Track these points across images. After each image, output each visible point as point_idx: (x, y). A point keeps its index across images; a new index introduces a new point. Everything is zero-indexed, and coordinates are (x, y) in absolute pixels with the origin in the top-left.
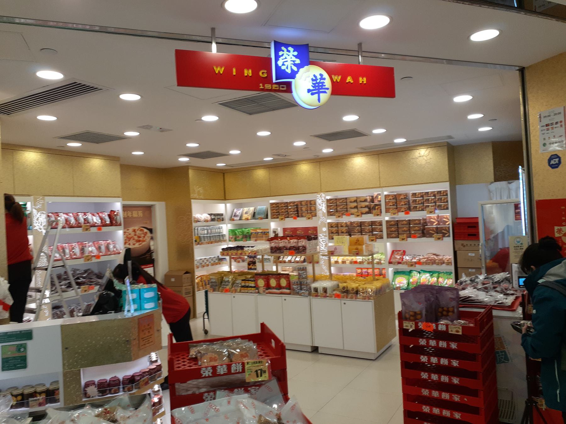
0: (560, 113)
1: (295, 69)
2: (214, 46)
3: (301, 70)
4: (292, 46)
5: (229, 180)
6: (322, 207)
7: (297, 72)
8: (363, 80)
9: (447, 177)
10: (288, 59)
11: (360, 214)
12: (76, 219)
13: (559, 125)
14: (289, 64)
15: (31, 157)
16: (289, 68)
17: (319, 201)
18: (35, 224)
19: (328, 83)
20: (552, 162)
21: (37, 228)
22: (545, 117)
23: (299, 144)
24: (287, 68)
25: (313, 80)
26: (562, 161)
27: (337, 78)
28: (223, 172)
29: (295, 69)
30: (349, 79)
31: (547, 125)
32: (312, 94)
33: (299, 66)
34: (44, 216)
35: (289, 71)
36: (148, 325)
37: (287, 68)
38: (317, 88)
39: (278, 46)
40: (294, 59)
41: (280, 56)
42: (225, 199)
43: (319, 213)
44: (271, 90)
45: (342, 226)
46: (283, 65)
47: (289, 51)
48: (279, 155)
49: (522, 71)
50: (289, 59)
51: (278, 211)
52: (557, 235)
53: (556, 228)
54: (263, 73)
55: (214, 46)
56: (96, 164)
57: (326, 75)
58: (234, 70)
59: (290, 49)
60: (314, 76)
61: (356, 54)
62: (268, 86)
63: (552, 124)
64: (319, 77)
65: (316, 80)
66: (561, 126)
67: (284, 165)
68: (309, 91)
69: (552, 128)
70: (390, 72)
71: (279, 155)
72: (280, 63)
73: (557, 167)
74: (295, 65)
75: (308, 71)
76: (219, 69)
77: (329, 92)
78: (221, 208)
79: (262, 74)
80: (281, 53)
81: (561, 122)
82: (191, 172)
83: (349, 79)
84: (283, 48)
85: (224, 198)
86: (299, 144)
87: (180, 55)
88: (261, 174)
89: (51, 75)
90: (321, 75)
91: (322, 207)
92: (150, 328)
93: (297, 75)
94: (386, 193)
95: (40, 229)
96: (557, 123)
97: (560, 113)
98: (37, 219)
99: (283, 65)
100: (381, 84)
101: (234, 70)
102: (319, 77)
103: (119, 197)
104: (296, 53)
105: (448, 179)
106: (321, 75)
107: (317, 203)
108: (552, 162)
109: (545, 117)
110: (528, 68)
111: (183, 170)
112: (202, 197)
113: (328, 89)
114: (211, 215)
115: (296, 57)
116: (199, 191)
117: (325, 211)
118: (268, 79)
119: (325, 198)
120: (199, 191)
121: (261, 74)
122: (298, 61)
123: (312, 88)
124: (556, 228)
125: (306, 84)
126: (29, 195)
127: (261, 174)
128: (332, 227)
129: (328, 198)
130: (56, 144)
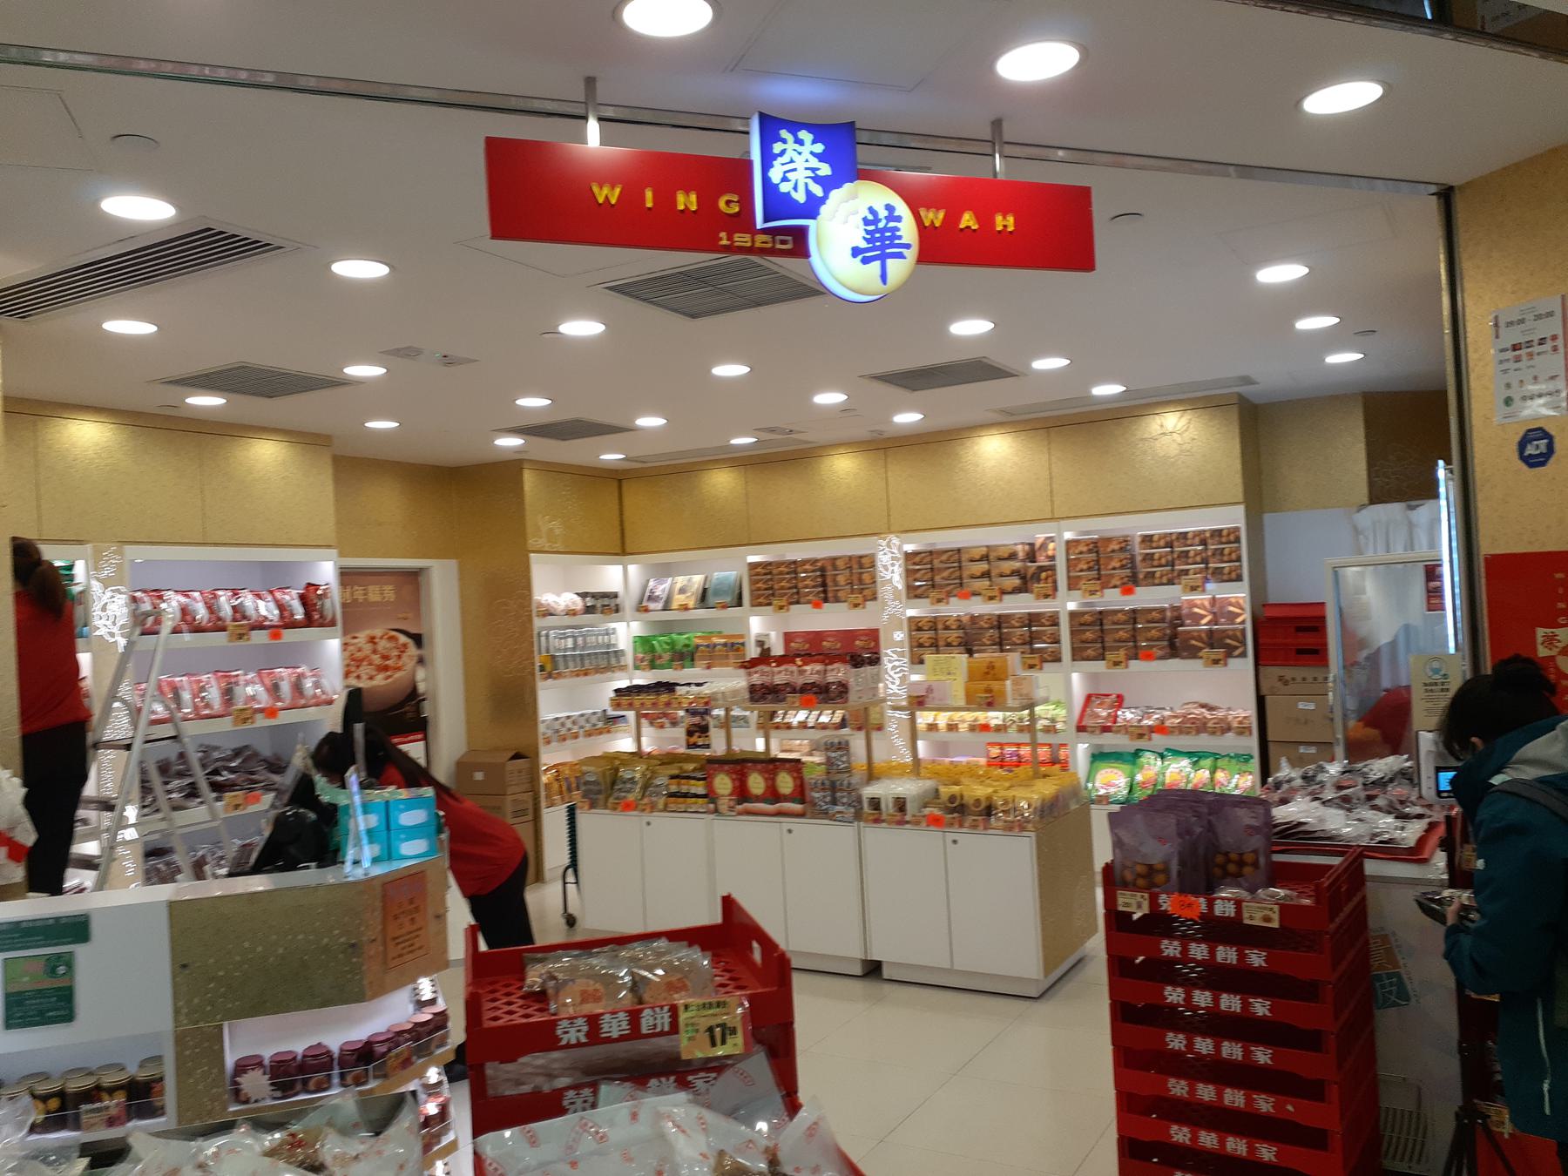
0: (1550, 314)
1: (817, 190)
2: (593, 128)
3: (835, 194)
4: (810, 128)
5: (635, 498)
6: (892, 574)
7: (823, 200)
8: (1005, 222)
9: (1237, 491)
10: (797, 165)
11: (996, 593)
12: (211, 608)
13: (1548, 346)
14: (801, 176)
15: (86, 435)
16: (801, 188)
17: (883, 559)
18: (97, 622)
19: (908, 230)
20: (1530, 450)
21: (102, 632)
22: (1509, 324)
23: (830, 398)
24: (795, 188)
25: (866, 222)
26: (1557, 445)
27: (935, 217)
28: (617, 478)
29: (817, 190)
30: (968, 220)
31: (1515, 348)
32: (865, 261)
33: (829, 184)
34: (121, 600)
35: (800, 197)
36: (411, 901)
37: (795, 188)
38: (878, 244)
39: (771, 127)
40: (814, 163)
41: (776, 157)
42: (624, 552)
43: (885, 592)
44: (751, 250)
45: (947, 628)
46: (785, 179)
47: (800, 142)
48: (772, 430)
49: (1446, 196)
50: (800, 163)
51: (771, 586)
52: (1543, 652)
53: (1541, 632)
54: (728, 203)
55: (593, 128)
56: (266, 454)
57: (902, 209)
58: (649, 194)
59: (804, 135)
60: (871, 210)
61: (987, 149)
62: (742, 239)
63: (1529, 344)
64: (883, 213)
65: (876, 221)
66: (1555, 349)
67: (788, 458)
68: (856, 252)
69: (1530, 355)
70: (1080, 199)
71: (772, 430)
72: (775, 175)
73: (1543, 464)
74: (817, 179)
75: (854, 197)
76: (606, 191)
77: (911, 254)
78: (612, 576)
79: (727, 204)
80: (777, 147)
81: (1554, 338)
82: (529, 478)
83: (968, 220)
84: (784, 134)
85: (622, 550)
86: (830, 398)
87: (500, 154)
88: (722, 482)
89: (140, 209)
90: (890, 208)
91: (892, 574)
92: (417, 909)
93: (824, 209)
94: (1068, 535)
95: (112, 635)
96: (1542, 341)
97: (1550, 314)
98: (104, 609)
99: (785, 179)
100: (1056, 233)
101: (649, 194)
102: (883, 213)
103: (329, 547)
104: (819, 148)
105: (1240, 497)
106: (890, 208)
107: (879, 564)
108: (1530, 450)
109: (1509, 324)
110: (1462, 188)
111: (507, 471)
112: (559, 546)
113: (908, 246)
114: (583, 595)
115: (820, 157)
116: (551, 530)
117: (900, 586)
118: (744, 220)
119: (900, 548)
120: (551, 530)
121: (722, 204)
122: (825, 170)
123: (864, 245)
124: (1541, 632)
125: (848, 234)
126: (80, 542)
127: (722, 482)
128: (919, 629)
129: (910, 548)
130: (156, 399)
